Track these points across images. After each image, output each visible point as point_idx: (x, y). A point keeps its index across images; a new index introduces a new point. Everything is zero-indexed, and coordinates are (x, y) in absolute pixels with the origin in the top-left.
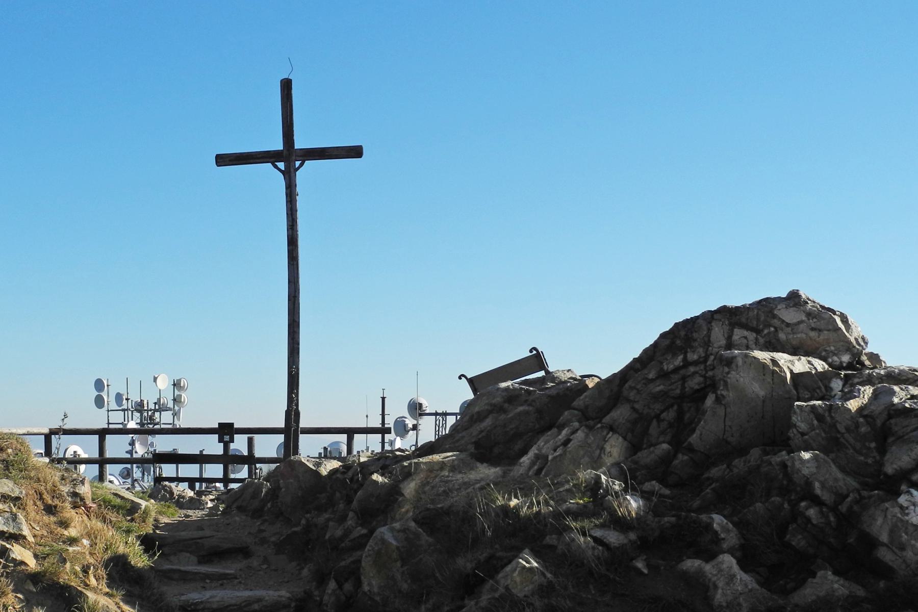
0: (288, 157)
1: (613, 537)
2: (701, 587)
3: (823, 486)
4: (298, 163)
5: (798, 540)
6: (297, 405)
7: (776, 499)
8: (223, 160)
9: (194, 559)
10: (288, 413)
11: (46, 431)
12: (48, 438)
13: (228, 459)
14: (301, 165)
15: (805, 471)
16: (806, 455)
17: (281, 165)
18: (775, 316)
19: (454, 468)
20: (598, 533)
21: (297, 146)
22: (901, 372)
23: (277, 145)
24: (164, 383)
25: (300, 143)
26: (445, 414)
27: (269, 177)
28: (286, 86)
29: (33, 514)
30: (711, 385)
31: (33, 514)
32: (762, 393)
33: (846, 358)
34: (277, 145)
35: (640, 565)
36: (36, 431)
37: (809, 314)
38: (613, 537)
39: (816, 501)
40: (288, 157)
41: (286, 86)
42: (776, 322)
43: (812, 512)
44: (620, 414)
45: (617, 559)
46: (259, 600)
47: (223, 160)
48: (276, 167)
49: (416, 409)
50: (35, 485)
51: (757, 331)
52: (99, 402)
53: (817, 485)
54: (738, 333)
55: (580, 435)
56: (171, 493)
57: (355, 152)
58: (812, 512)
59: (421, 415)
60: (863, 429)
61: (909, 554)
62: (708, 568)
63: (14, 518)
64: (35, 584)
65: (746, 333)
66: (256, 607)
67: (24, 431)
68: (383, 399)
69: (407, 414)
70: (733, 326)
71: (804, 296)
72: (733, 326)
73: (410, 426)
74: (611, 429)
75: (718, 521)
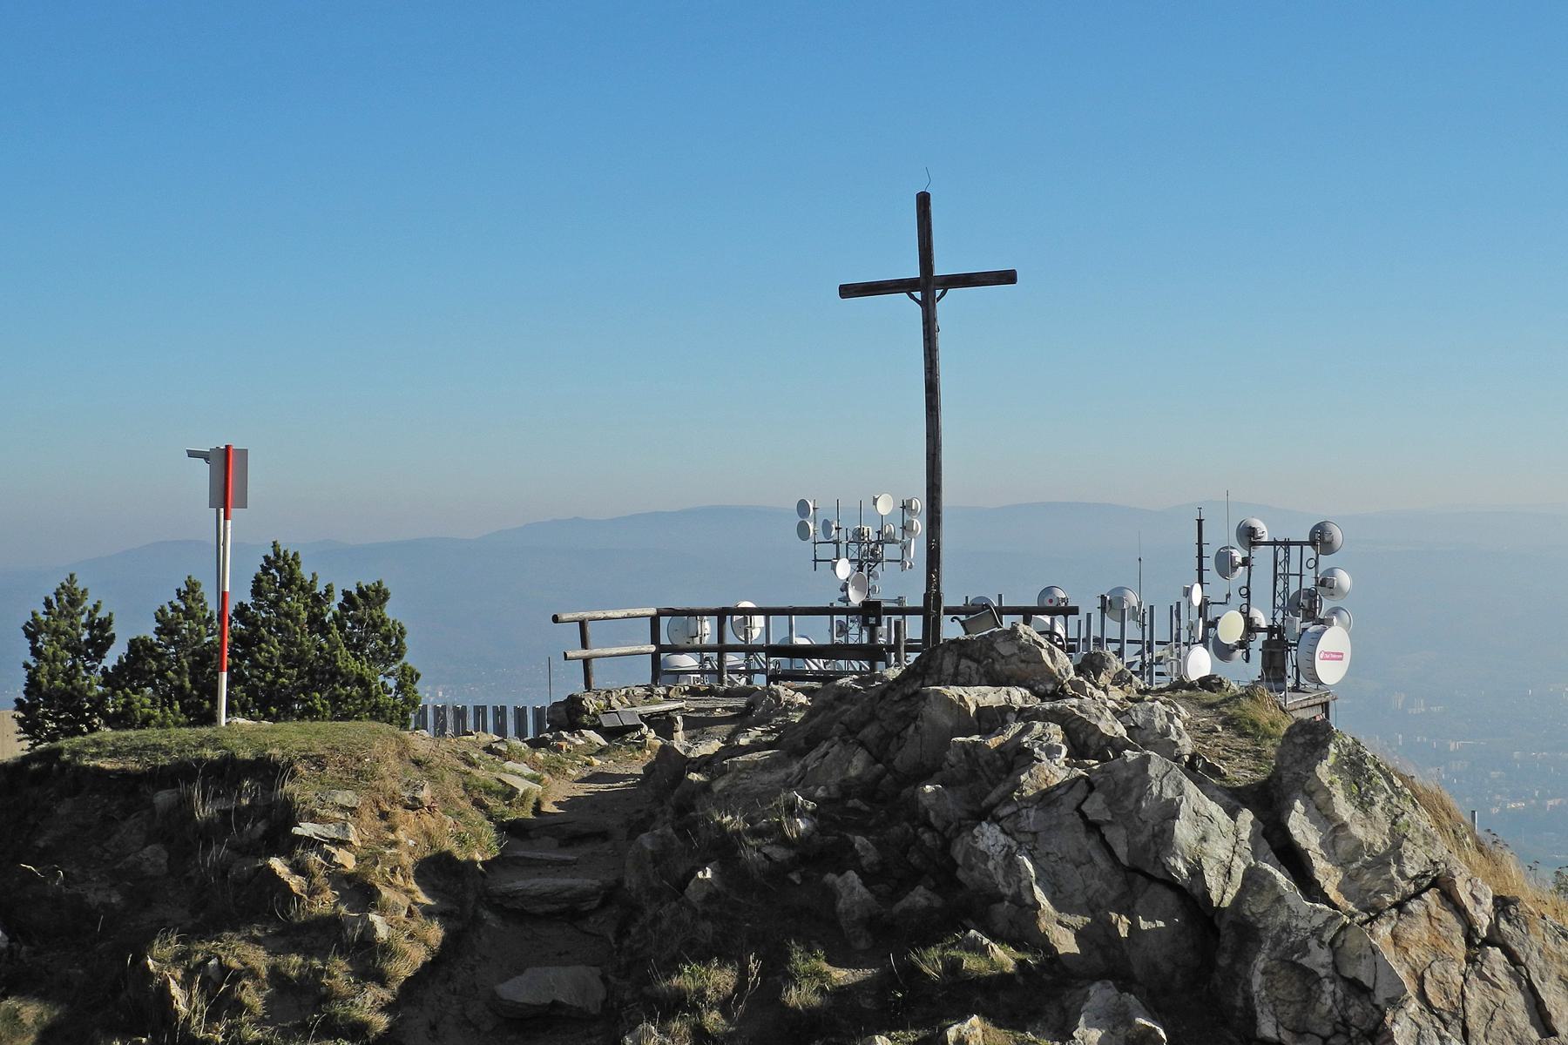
0: (927, 286)
1: (779, 854)
2: (831, 894)
3: (937, 815)
4: (938, 292)
5: (915, 859)
6: (938, 587)
7: (906, 824)
8: (847, 291)
9: (555, 842)
10: (927, 597)
11: (653, 611)
12: (655, 621)
13: (873, 653)
14: (943, 294)
15: (926, 803)
16: (929, 788)
17: (918, 295)
18: (994, 649)
19: (766, 767)
20: (766, 850)
21: (938, 272)
22: (585, 830)
23: (914, 272)
24: (885, 506)
25: (940, 270)
26: (1287, 544)
27: (906, 308)
28: (924, 201)
29: (367, 819)
30: (910, 718)
31: (367, 819)
32: (950, 724)
33: (1050, 687)
34: (914, 272)
35: (795, 877)
36: (638, 612)
37: (1022, 648)
38: (779, 854)
39: (929, 826)
40: (927, 286)
41: (924, 201)
42: (994, 654)
43: (926, 836)
44: (870, 732)
45: (777, 872)
46: (571, 888)
47: (847, 291)
48: (912, 297)
49: (1249, 536)
50: (374, 794)
51: (978, 662)
52: (803, 531)
53: (932, 814)
54: (964, 663)
55: (836, 748)
56: (778, 699)
57: (1008, 277)
58: (926, 836)
59: (1254, 544)
60: (999, 763)
61: (976, 874)
62: (839, 881)
63: (345, 827)
64: (349, 883)
65: (970, 663)
66: (567, 894)
67: (624, 613)
68: (1200, 521)
69: (1234, 541)
70: (960, 656)
71: (1168, 584)
72: (960, 656)
73: (1239, 560)
74: (862, 744)
75: (859, 841)
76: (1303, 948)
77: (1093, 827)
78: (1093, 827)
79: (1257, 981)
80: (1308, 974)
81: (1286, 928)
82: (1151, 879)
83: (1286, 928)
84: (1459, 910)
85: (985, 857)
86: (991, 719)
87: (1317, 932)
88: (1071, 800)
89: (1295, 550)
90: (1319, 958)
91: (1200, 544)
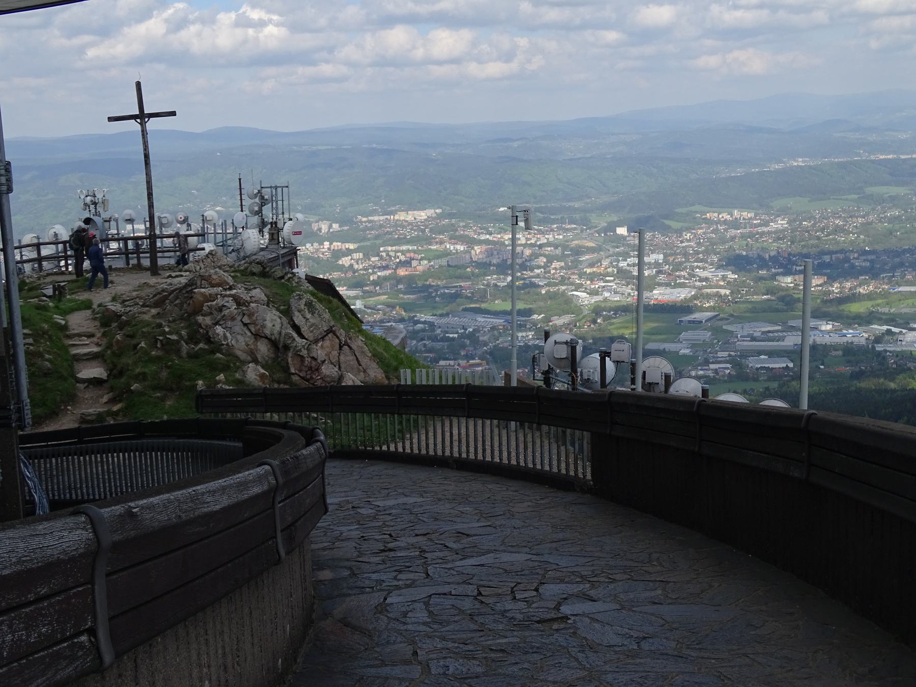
0: (142, 117)
26: (276, 188)
27: (134, 125)
40: (142, 117)
54: (203, 282)
76: (300, 350)
77: (245, 325)
78: (245, 325)
79: (290, 359)
80: (302, 357)
81: (296, 346)
82: (261, 337)
83: (296, 346)
84: (338, 337)
85: (218, 335)
86: (212, 298)
87: (303, 346)
88: (239, 318)
89: (279, 190)
90: (304, 352)
91: (240, 189)
